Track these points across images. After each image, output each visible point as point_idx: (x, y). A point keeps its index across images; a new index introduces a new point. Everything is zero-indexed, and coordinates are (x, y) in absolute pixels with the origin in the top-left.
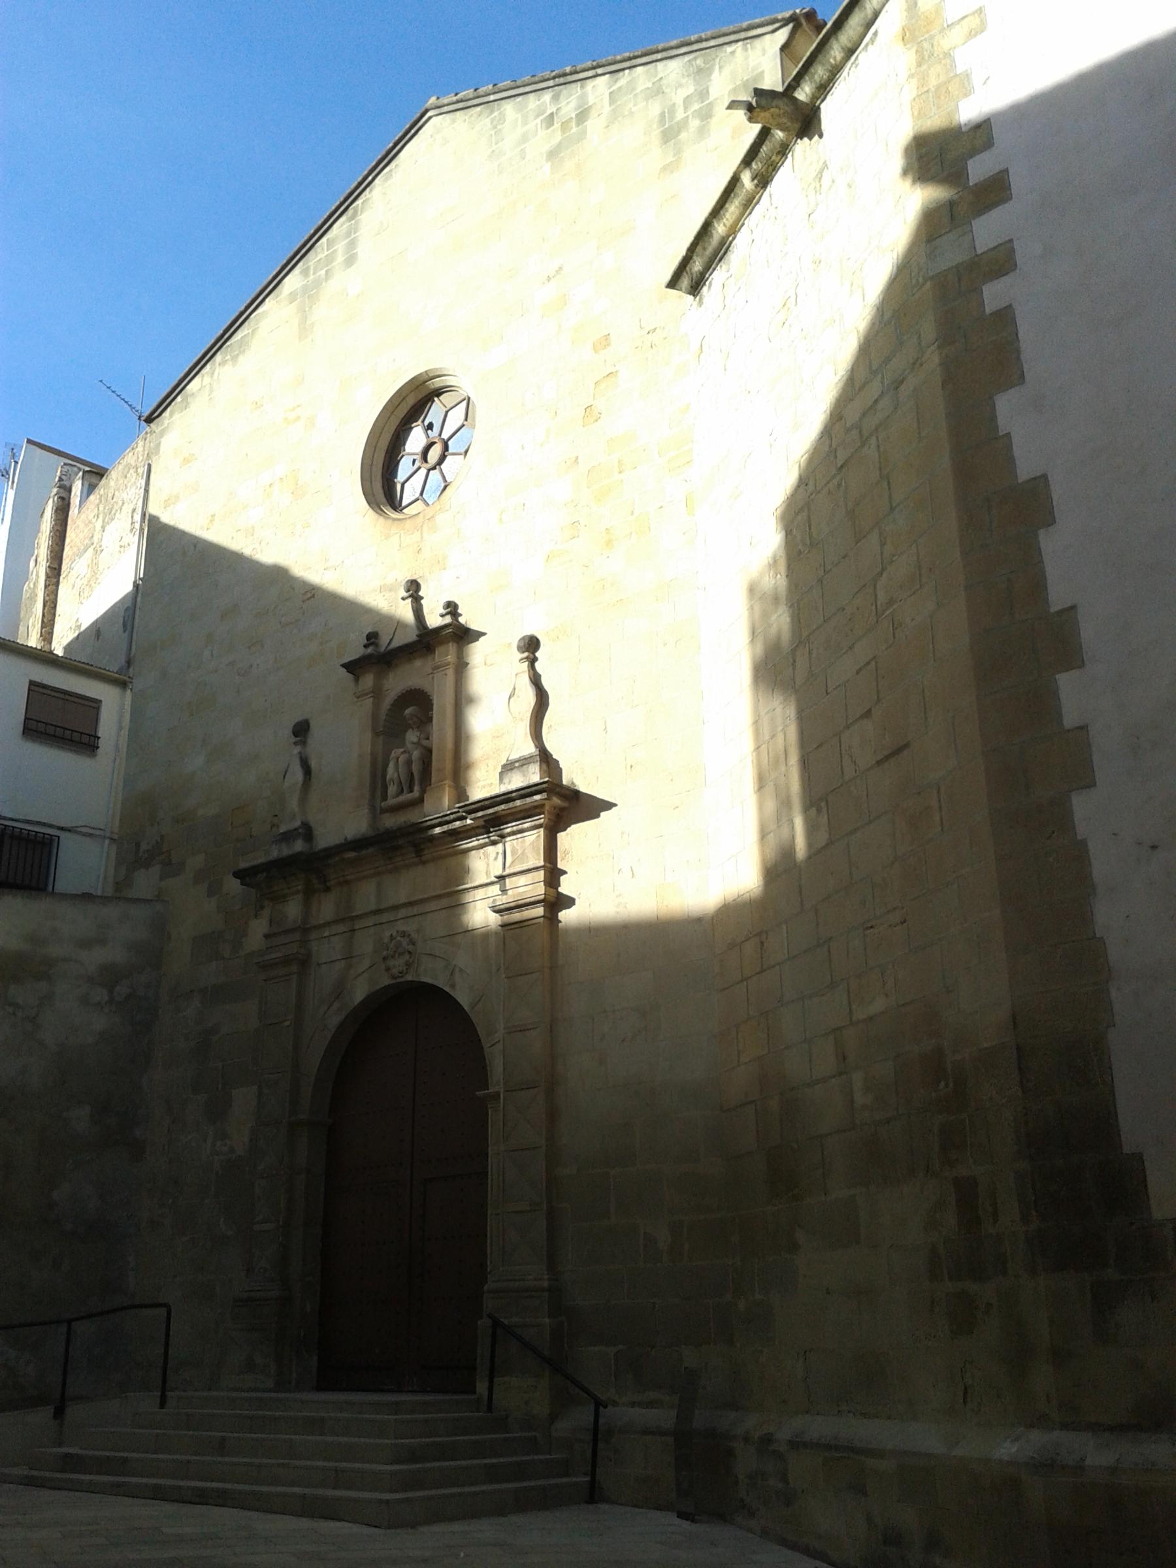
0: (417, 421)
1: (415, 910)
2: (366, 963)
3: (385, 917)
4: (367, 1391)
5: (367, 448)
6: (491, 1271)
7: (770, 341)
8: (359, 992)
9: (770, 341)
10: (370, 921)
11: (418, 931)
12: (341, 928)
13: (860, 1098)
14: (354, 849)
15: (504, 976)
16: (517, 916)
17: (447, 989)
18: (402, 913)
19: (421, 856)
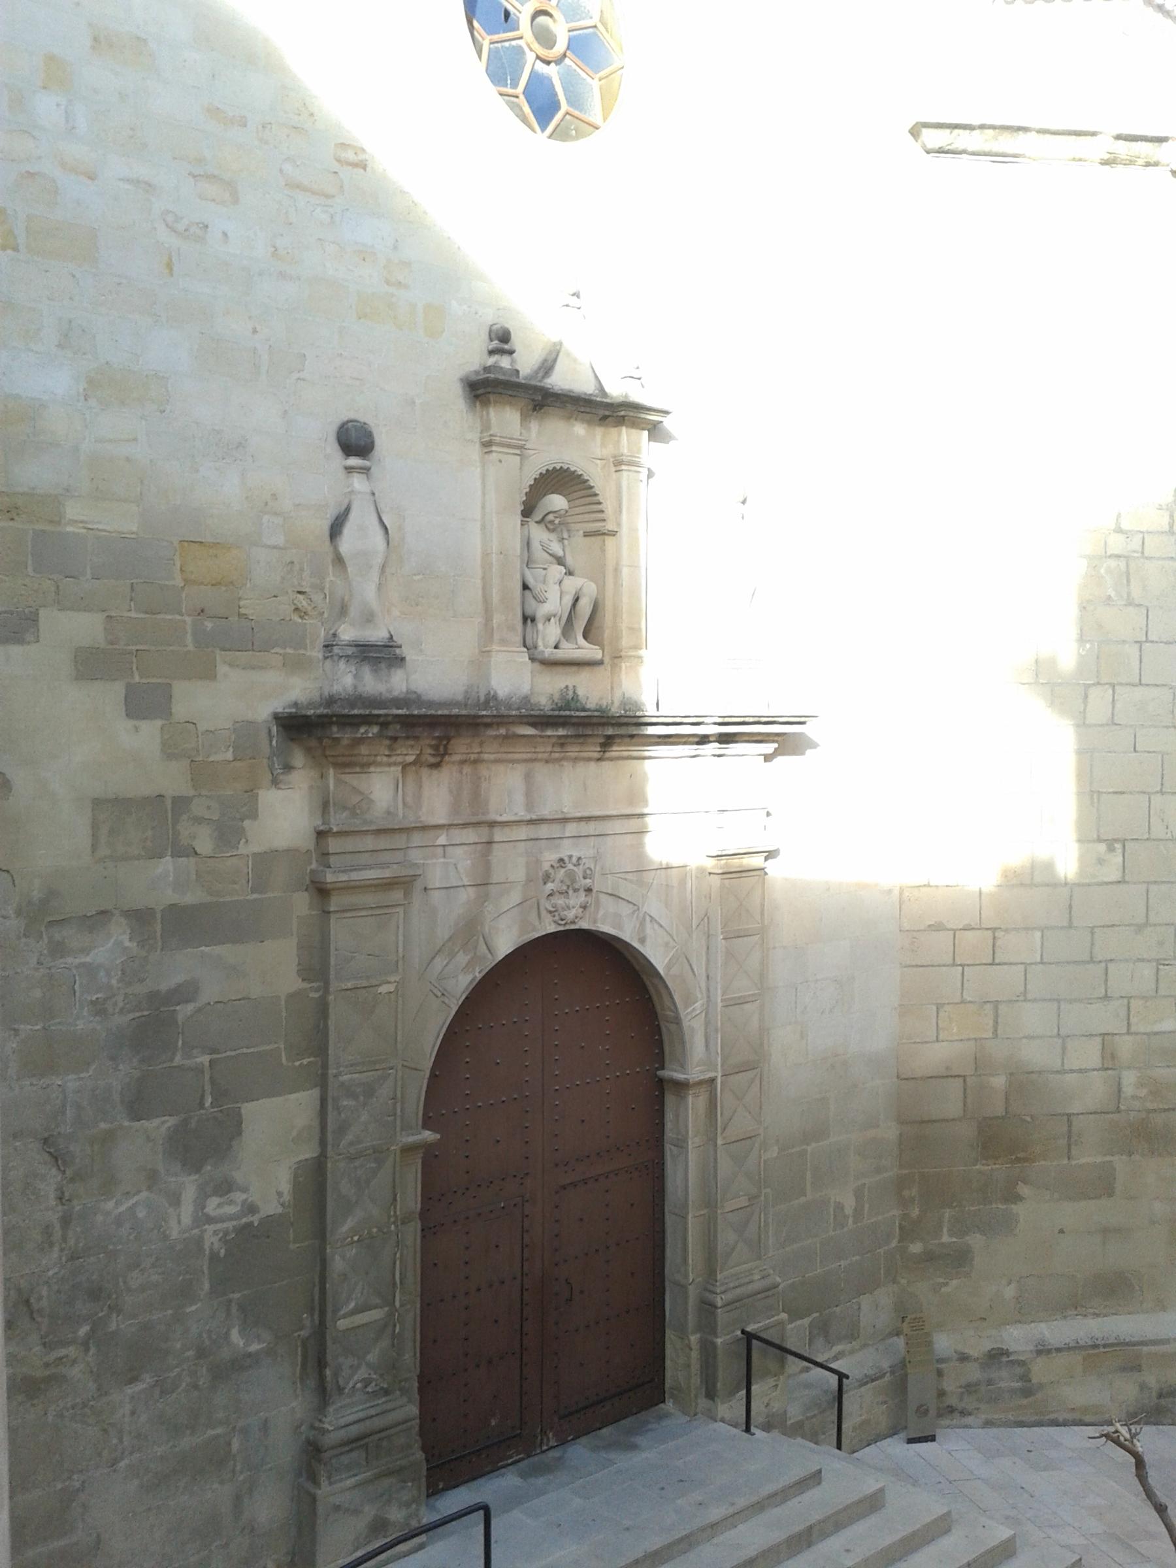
0: (550, 80)
1: (591, 828)
2: (515, 897)
3: (544, 831)
4: (458, 1486)
5: (468, 13)
6: (693, 1280)
7: (643, 387)
8: (504, 945)
9: (643, 387)
10: (523, 833)
11: (596, 859)
12: (470, 835)
13: (1128, 1090)
14: (533, 725)
15: (721, 937)
16: (736, 862)
17: (636, 944)
18: (571, 829)
19: (604, 752)
